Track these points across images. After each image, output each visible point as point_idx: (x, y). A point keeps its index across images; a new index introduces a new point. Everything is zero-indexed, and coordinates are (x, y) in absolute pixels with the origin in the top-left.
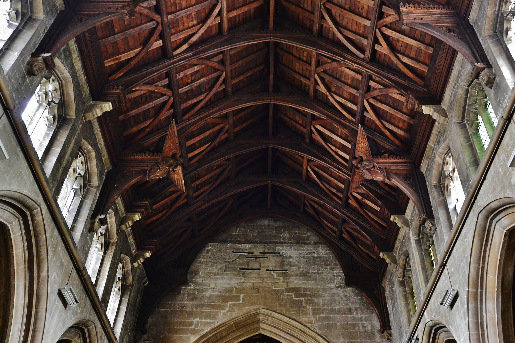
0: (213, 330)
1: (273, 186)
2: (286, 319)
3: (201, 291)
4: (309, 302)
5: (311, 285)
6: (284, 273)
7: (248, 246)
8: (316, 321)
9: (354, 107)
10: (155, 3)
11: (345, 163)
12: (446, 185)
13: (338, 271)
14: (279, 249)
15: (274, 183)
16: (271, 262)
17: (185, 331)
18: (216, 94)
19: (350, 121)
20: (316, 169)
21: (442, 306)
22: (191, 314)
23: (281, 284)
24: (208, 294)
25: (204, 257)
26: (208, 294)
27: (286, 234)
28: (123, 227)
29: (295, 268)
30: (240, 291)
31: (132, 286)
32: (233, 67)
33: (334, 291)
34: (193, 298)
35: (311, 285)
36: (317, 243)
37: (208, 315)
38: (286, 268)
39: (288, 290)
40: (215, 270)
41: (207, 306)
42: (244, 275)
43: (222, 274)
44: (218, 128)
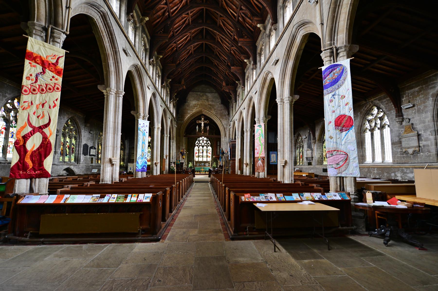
0: (193, 114)
1: (205, 43)
2: (208, 111)
3: (189, 104)
4: (213, 108)
5: (213, 103)
6: (208, 100)
7: (199, 93)
8: (214, 112)
9: (236, 15)
10: (165, 1)
11: (230, 36)
12: (286, 6)
13: (220, 100)
14: (206, 94)
15: (206, 42)
16: (204, 97)
17: (187, 114)
18: (188, 40)
19: (227, 52)
20: (223, 21)
21: (309, 3)
22: (188, 110)
23: (206, 103)
24: (191, 105)
25: (189, 96)
26: (191, 105)
27: (208, 89)
28: (167, 83)
29: (210, 99)
30: (198, 105)
31: (139, 27)
32: (191, 14)
33: (219, 105)
34: (188, 106)
35: (213, 103)
36: (215, 93)
37: (191, 110)
38: (208, 99)
39: (208, 105)
40: (192, 99)
41: (191, 108)
42: (198, 101)
43: (193, 100)
44: (185, 19)
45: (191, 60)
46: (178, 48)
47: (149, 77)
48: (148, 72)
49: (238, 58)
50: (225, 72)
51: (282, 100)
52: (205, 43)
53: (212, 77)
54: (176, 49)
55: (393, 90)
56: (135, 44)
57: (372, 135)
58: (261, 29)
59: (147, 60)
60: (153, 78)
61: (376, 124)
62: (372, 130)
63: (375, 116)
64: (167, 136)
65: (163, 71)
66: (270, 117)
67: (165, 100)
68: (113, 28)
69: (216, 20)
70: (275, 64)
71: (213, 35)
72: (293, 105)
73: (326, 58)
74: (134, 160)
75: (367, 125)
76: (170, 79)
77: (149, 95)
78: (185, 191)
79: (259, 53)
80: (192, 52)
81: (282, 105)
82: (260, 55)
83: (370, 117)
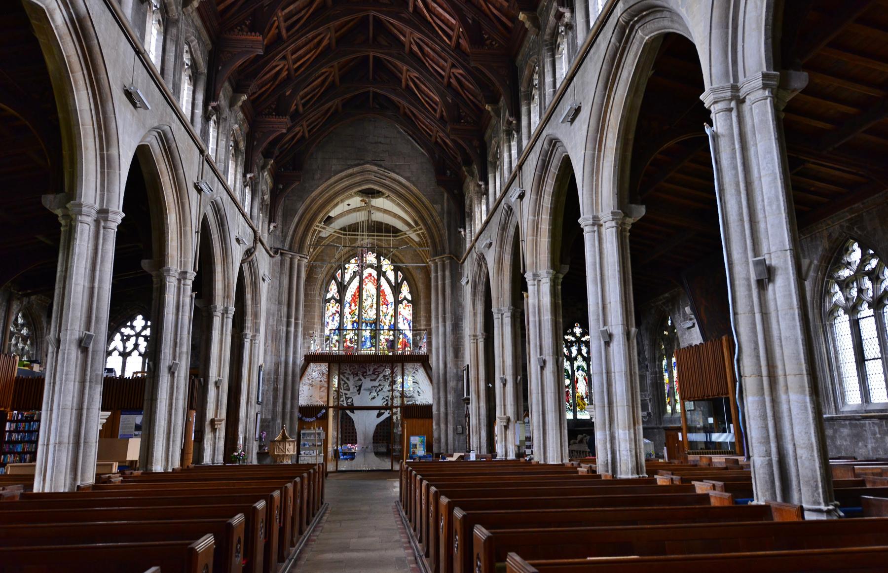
12: (558, 43)
45: (330, 104)
46: (293, 72)
47: (243, 215)
49: (453, 155)
51: (596, 222)
52: (374, 57)
57: (855, 326)
58: (492, 114)
61: (860, 291)
62: (852, 310)
63: (855, 267)
64: (226, 310)
65: (250, 138)
66: (566, 269)
69: (400, 75)
71: (395, 70)
72: (628, 234)
73: (716, 105)
74: (640, 409)
75: (838, 296)
77: (237, 253)
78: (275, 557)
80: (334, 81)
82: (530, 98)
83: (845, 273)
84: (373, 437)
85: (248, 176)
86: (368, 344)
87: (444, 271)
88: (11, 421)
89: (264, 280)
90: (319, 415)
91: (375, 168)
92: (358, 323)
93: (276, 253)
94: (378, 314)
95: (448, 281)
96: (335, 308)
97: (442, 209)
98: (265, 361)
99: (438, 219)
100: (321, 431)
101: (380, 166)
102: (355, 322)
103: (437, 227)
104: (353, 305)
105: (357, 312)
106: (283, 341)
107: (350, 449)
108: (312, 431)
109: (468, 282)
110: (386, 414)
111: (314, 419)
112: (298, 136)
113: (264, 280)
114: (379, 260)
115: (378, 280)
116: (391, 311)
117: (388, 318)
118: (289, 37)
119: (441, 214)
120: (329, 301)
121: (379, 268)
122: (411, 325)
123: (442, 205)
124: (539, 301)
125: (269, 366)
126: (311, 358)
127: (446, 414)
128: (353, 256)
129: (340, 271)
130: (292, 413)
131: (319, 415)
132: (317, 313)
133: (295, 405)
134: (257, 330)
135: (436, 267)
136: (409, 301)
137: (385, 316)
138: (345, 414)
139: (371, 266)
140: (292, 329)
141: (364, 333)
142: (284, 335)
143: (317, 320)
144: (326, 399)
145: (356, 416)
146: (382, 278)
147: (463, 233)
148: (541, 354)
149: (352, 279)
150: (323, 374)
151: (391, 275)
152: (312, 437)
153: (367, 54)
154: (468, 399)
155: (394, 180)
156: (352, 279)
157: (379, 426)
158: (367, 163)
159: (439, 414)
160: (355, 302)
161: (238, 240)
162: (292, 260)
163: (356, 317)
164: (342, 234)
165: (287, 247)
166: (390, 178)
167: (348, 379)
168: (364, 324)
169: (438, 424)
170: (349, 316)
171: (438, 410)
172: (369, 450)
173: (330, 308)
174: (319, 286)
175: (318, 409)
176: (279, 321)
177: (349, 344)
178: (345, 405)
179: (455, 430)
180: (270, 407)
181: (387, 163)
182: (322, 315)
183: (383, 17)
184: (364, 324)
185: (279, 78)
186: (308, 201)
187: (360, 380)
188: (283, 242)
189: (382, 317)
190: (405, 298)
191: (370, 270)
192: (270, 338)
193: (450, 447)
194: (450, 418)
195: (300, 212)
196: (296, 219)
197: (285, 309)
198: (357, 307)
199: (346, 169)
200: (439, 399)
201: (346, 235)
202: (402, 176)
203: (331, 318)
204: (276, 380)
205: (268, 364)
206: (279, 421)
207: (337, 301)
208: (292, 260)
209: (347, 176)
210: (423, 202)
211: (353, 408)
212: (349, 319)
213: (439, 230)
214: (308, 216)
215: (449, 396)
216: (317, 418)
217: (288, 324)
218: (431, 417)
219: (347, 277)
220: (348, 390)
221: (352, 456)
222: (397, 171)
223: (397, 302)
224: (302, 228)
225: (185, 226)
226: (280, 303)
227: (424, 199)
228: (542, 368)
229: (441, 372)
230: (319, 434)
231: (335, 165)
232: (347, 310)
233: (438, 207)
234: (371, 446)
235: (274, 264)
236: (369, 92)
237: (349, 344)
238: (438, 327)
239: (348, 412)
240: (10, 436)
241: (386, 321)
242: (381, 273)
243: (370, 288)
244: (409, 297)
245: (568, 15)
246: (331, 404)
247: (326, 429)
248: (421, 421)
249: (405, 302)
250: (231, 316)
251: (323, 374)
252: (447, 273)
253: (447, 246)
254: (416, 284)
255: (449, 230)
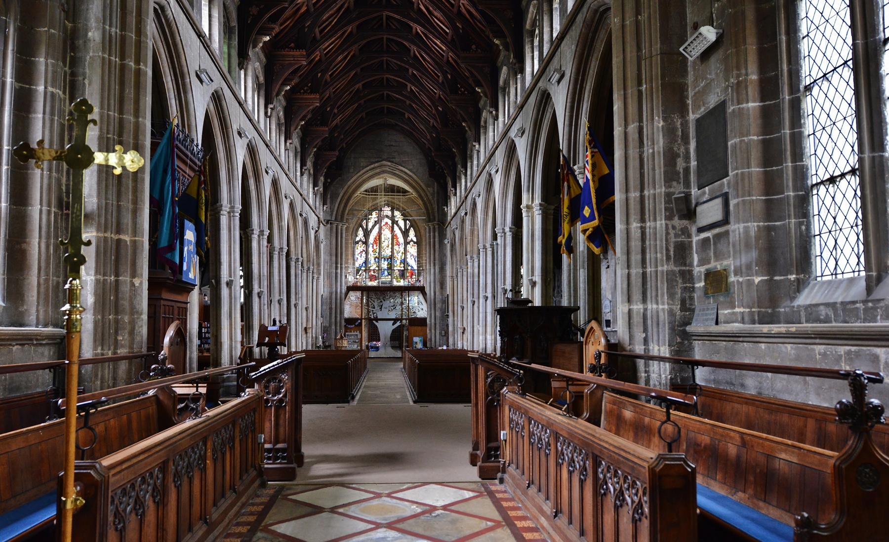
48: (194, 15)
49: (480, 28)
50: (456, 6)
52: (387, 94)
53: (411, 28)
54: (307, 11)
55: (286, 377)
56: (210, 34)
59: (311, 190)
60: (280, 155)
67: (251, 108)
68: (180, 37)
70: (520, 135)
76: (266, 35)
79: (501, 88)
80: (348, 7)
81: (530, 218)
84: (391, 337)
85: (316, 189)
86: (386, 273)
87: (434, 232)
88: (205, 328)
89: (267, 172)
90: (357, 324)
91: (389, 164)
92: (378, 258)
93: (327, 223)
94: (392, 252)
95: (437, 240)
96: (362, 248)
97: (434, 191)
98: (324, 292)
99: (431, 197)
100: (358, 333)
101: (392, 162)
102: (376, 257)
103: (430, 202)
104: (375, 245)
105: (378, 250)
106: (334, 279)
107: (376, 345)
108: (353, 333)
109: (497, 171)
110: (398, 324)
111: (354, 326)
112: (317, 59)
113: (267, 172)
114: (393, 213)
115: (393, 227)
116: (402, 249)
117: (400, 254)
118: (322, 38)
119: (433, 194)
120: (357, 243)
121: (392, 218)
122: (416, 259)
123: (434, 188)
124: (473, 271)
125: (326, 295)
126: (351, 289)
127: (435, 324)
128: (374, 210)
129: (365, 221)
130: (340, 323)
131: (357, 324)
132: (350, 252)
133: (343, 318)
134: (320, 274)
135: (430, 229)
136: (414, 243)
137: (398, 253)
138: (372, 323)
139: (387, 216)
140: (339, 271)
141: (383, 266)
142: (334, 275)
143: (350, 257)
144: (360, 313)
145: (380, 325)
146: (395, 225)
147: (446, 209)
148: (473, 298)
149: (373, 227)
150: (358, 298)
151: (401, 223)
152: (353, 337)
153: (383, 106)
154: (448, 315)
155: (402, 171)
156: (373, 227)
157: (394, 331)
158: (384, 160)
159: (431, 324)
160: (376, 243)
161: (239, 134)
162: (337, 227)
163: (377, 254)
164: (366, 195)
165: (333, 218)
166: (399, 169)
167: (374, 301)
168: (383, 259)
169: (430, 330)
170: (372, 253)
171: (431, 321)
172: (387, 345)
173: (359, 247)
174: (351, 233)
175: (356, 320)
176: (331, 266)
177: (372, 273)
178: (372, 317)
179: (440, 333)
180: (328, 319)
181: (397, 160)
182: (354, 255)
183: (390, 93)
184: (383, 259)
185: (300, 13)
186: (346, 187)
187: (381, 302)
188: (331, 215)
189: (395, 254)
190: (412, 240)
191: (386, 220)
192: (326, 277)
193: (438, 343)
194: (438, 326)
195: (341, 195)
196: (339, 200)
197: (334, 258)
198: (378, 247)
199: (370, 165)
200: (431, 314)
201: (369, 195)
202: (407, 168)
203: (360, 255)
204: (331, 303)
205: (326, 293)
206: (333, 327)
207: (363, 243)
208: (337, 227)
209: (370, 170)
210: (421, 186)
211: (377, 320)
212: (372, 256)
213: (432, 205)
214: (346, 197)
215: (437, 313)
216: (355, 325)
217: (336, 268)
218: (426, 325)
219: (370, 225)
220: (374, 308)
221: (377, 349)
222: (403, 165)
223: (406, 243)
224: (343, 205)
225: (297, 235)
226: (331, 255)
227: (422, 184)
228: (473, 305)
229: (432, 298)
230: (357, 335)
231: (363, 162)
232: (370, 249)
233: (430, 189)
234: (389, 343)
235: (327, 230)
236: (384, 107)
237: (372, 273)
238: (430, 269)
239: (374, 322)
240: (205, 335)
241: (399, 257)
242: (394, 222)
243: (387, 234)
244: (415, 239)
245: (477, 146)
246: (363, 317)
247: (361, 333)
248: (420, 328)
249: (412, 243)
250: (237, 215)
251: (358, 298)
252: (437, 234)
253: (436, 215)
254: (419, 231)
255: (438, 205)
